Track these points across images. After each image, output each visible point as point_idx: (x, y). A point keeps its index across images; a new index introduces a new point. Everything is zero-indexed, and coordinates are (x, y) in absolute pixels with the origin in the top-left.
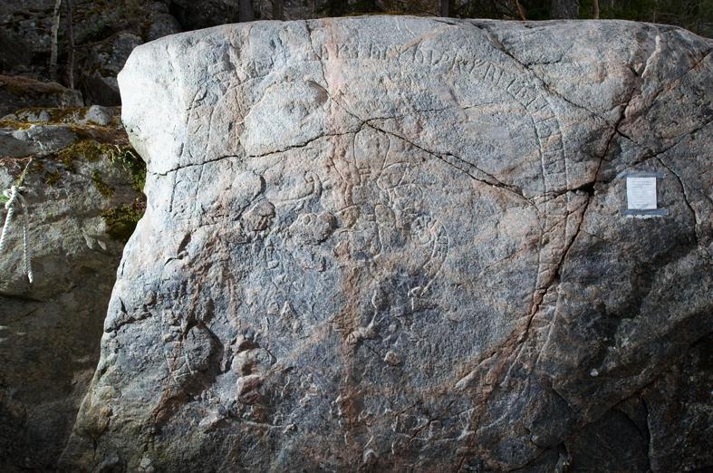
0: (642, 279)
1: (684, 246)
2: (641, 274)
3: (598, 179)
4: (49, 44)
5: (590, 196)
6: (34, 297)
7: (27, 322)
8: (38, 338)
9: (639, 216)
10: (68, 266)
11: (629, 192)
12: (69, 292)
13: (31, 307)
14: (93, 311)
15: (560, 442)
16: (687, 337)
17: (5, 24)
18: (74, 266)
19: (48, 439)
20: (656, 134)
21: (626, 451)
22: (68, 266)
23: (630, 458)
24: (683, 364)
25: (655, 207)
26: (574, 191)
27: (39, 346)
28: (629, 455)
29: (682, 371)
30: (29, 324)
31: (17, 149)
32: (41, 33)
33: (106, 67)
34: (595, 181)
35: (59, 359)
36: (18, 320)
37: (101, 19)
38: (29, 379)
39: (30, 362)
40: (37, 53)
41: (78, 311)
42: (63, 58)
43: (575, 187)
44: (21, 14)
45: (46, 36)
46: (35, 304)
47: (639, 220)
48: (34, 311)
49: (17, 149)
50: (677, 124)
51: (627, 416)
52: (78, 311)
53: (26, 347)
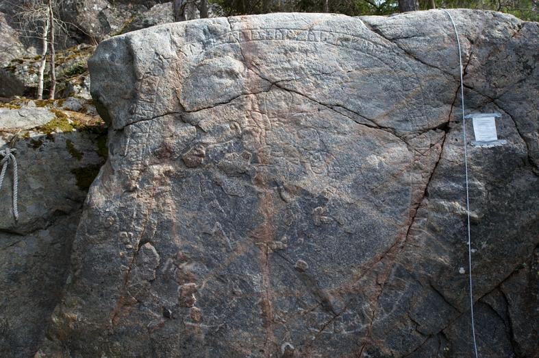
0: (492, 194)
1: (521, 168)
2: (491, 191)
3: (451, 120)
4: (37, 82)
5: (446, 133)
6: (17, 231)
7: (11, 251)
8: (19, 263)
9: (485, 146)
10: (45, 208)
11: (476, 128)
12: (46, 229)
13: (15, 239)
14: (64, 245)
15: (440, 330)
16: (531, 239)
17: (5, 68)
18: (51, 209)
19: (24, 345)
20: (492, 85)
21: (494, 337)
22: (45, 208)
23: (497, 343)
24: (531, 262)
25: (496, 139)
26: (434, 129)
27: (20, 270)
28: (495, 340)
29: (531, 267)
30: (13, 253)
31: (10, 123)
32: (31, 73)
33: (79, 95)
34: (449, 122)
35: (37, 281)
36: (5, 249)
37: (76, 62)
38: (12, 296)
39: (13, 283)
40: (28, 87)
41: (52, 244)
42: (48, 86)
43: (435, 126)
44: (16, 60)
45: (35, 75)
46: (18, 237)
47: (485, 149)
48: (18, 242)
49: (10, 123)
50: (506, 77)
51: (491, 307)
52: (52, 244)
53: (10, 270)
